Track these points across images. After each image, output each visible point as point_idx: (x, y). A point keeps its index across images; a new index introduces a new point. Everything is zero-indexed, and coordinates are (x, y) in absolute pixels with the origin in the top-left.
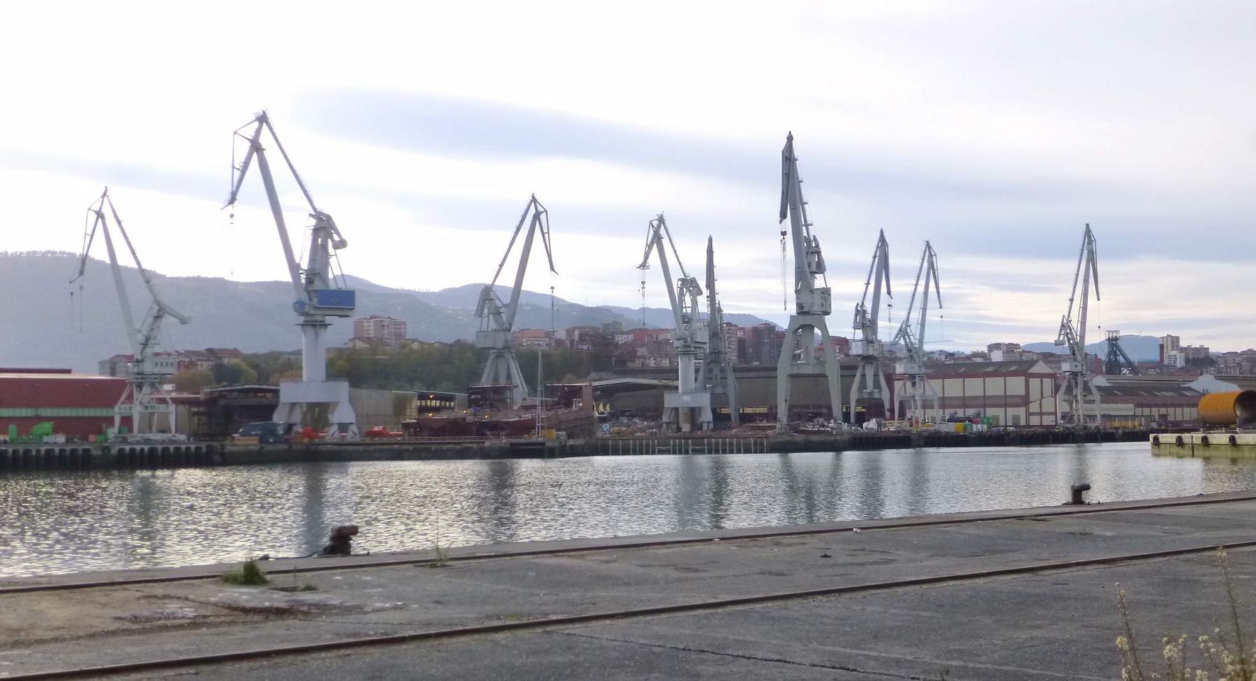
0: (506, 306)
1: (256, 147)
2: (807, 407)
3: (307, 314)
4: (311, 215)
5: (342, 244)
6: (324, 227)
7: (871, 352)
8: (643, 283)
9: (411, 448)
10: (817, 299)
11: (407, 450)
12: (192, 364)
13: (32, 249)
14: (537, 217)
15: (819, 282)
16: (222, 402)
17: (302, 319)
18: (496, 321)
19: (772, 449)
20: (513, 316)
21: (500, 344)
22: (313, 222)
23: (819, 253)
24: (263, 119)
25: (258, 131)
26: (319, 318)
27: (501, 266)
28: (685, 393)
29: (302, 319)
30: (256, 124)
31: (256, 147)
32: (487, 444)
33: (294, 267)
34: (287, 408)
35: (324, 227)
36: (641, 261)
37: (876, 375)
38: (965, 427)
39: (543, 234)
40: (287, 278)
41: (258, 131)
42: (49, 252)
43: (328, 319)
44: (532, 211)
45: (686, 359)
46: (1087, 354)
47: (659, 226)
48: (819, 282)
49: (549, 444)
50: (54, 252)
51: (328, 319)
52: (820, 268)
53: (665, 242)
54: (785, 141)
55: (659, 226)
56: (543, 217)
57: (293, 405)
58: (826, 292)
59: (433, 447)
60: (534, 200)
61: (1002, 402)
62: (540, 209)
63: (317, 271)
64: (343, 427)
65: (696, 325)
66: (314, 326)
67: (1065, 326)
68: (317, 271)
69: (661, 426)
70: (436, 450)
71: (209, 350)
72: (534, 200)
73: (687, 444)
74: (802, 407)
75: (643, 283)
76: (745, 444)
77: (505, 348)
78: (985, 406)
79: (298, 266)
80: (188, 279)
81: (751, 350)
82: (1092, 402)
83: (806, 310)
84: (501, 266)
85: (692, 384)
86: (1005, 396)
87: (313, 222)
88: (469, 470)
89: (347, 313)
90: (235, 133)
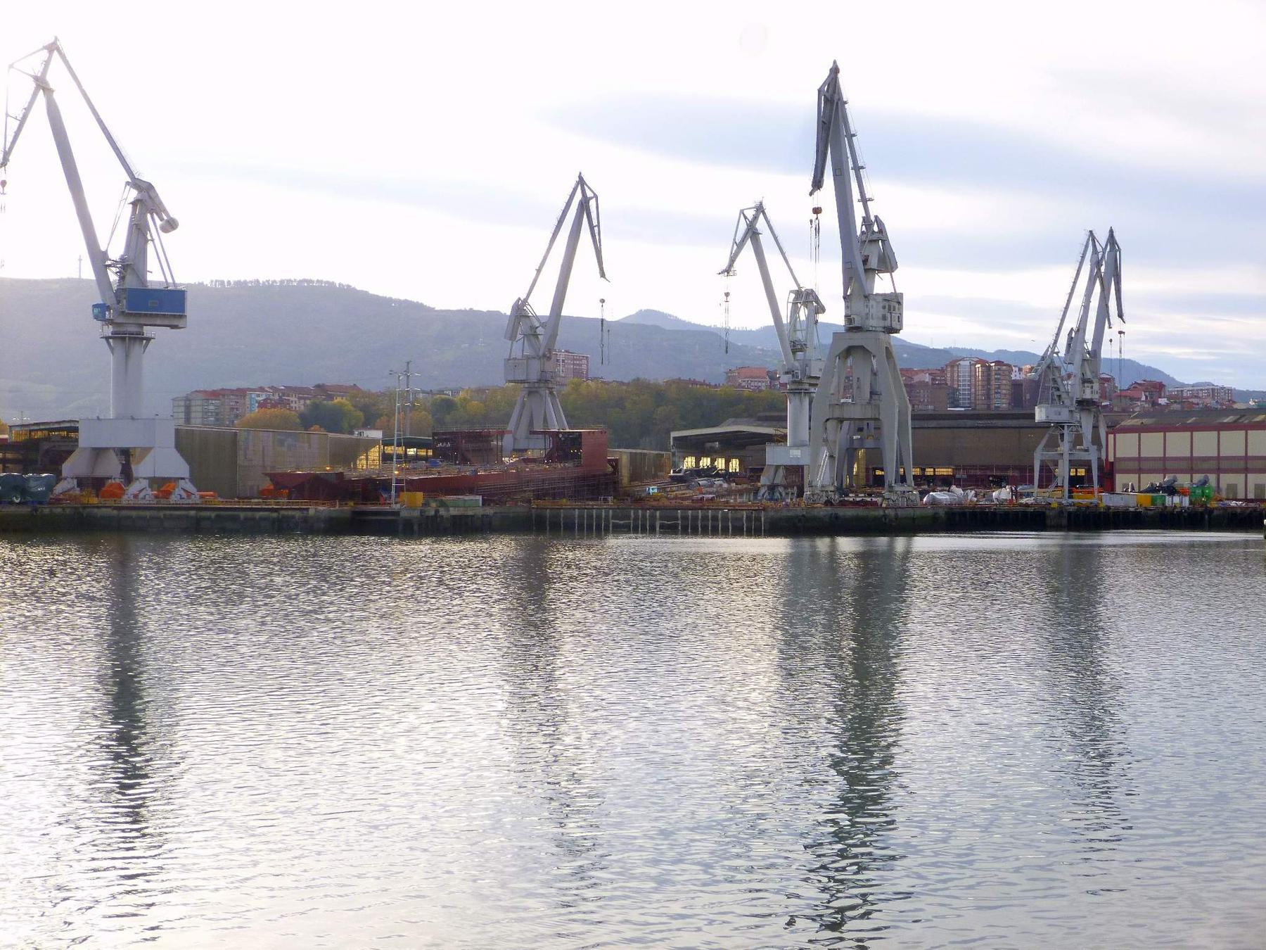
0: (543, 325)
1: (41, 84)
2: (989, 468)
3: (110, 322)
4: (128, 183)
5: (171, 225)
6: (146, 201)
7: (1088, 395)
8: (727, 295)
9: (213, 514)
10: (876, 310)
11: (209, 518)
12: (282, 403)
13: (286, 277)
14: (584, 206)
15: (882, 284)
16: (46, 446)
17: (109, 330)
18: (531, 345)
19: (774, 529)
20: (553, 336)
21: (534, 376)
22: (133, 194)
23: (885, 241)
24: (53, 48)
25: (47, 64)
26: (133, 329)
27: (539, 271)
28: (796, 446)
29: (109, 330)
30: (45, 54)
31: (41, 84)
32: (312, 512)
33: (99, 259)
34: (772, 470)
35: (146, 201)
36: (724, 267)
37: (1095, 427)
38: (1153, 501)
39: (592, 228)
40: (89, 273)
41: (47, 64)
42: (305, 281)
43: (148, 331)
44: (578, 196)
45: (796, 399)
46: (907, 372)
47: (756, 218)
48: (882, 284)
49: (404, 514)
50: (311, 281)
51: (148, 331)
52: (887, 263)
53: (765, 238)
54: (827, 73)
55: (756, 218)
56: (592, 203)
57: (777, 467)
58: (893, 302)
59: (242, 515)
60: (581, 182)
61: (1242, 465)
62: (589, 194)
63: (132, 264)
64: (162, 485)
65: (810, 353)
66: (123, 339)
67: (1075, 338)
68: (132, 264)
69: (757, 491)
70: (246, 519)
71: (318, 386)
72: (581, 182)
73: (653, 517)
74: (998, 468)
75: (727, 295)
76: (735, 519)
77: (539, 381)
78: (1219, 471)
79: (105, 255)
80: (460, 311)
81: (1028, 396)
82: (1074, 464)
83: (856, 324)
84: (539, 271)
85: (804, 434)
86: (1246, 458)
87: (133, 194)
88: (502, 548)
89: (175, 322)
90: (11, 66)
